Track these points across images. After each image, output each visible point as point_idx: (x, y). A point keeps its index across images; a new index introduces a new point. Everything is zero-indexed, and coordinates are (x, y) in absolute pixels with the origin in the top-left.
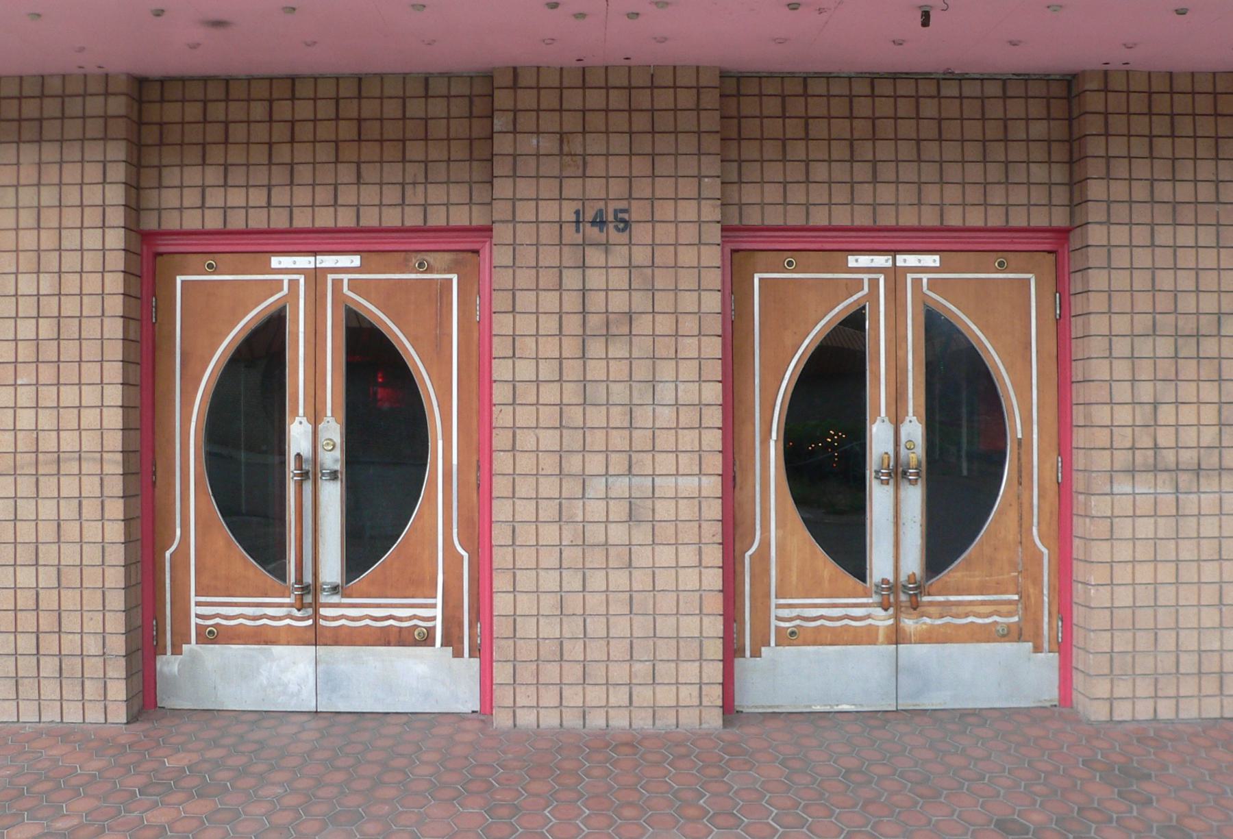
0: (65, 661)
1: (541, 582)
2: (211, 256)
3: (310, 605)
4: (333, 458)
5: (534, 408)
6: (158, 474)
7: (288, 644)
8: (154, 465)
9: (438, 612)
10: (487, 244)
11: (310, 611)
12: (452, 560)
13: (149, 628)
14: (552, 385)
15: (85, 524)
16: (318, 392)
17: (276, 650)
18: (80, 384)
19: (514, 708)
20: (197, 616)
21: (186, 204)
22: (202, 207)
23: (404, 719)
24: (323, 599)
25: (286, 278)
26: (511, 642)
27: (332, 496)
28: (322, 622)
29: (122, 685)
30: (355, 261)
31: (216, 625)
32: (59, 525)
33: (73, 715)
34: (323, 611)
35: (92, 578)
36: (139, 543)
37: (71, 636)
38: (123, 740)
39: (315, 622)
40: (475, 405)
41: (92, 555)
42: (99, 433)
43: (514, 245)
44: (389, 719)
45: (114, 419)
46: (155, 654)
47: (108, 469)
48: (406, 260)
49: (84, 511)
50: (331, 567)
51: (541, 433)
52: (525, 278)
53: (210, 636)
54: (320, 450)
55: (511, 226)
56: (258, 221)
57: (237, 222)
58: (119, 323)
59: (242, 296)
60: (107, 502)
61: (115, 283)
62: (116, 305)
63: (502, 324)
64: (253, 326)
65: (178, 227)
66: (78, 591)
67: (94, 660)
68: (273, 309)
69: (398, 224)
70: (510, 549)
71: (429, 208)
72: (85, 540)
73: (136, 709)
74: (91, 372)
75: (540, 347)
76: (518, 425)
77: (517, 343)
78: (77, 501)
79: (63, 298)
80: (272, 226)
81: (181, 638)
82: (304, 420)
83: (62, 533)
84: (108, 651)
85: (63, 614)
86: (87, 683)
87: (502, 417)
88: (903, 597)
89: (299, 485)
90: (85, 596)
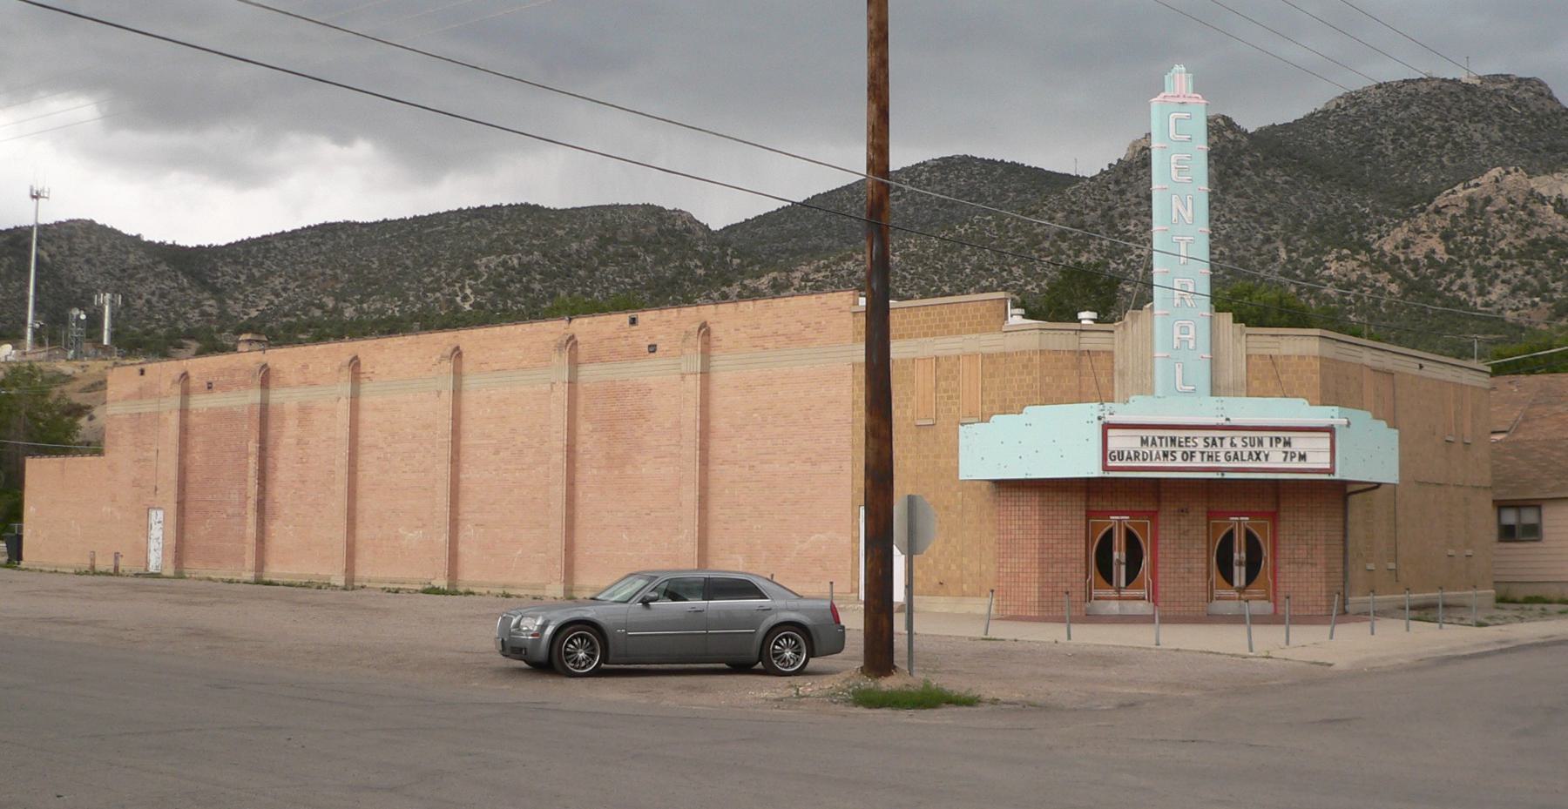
4: (1123, 560)
27: (1123, 568)
50: (1123, 584)
59: (1104, 525)
88: (1241, 590)
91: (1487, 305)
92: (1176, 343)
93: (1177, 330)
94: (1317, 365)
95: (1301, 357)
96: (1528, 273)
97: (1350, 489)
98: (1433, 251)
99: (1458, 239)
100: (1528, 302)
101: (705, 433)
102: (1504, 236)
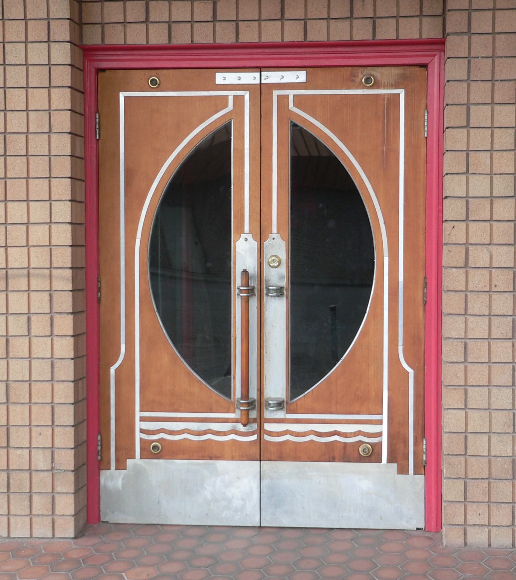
0: (13, 476)
1: (493, 399)
2: (154, 72)
3: (254, 421)
4: (278, 275)
5: (487, 224)
6: (103, 291)
7: (233, 459)
8: (99, 281)
9: (384, 428)
10: (436, 59)
11: (255, 426)
12: (398, 378)
13: (96, 442)
14: (506, 201)
15: (34, 340)
16: (264, 209)
17: (221, 465)
18: (27, 200)
19: (465, 526)
20: (142, 431)
21: (129, 19)
22: (147, 21)
23: (349, 535)
24: (267, 414)
25: (231, 94)
26: (462, 459)
27: (277, 313)
28: (267, 438)
29: (71, 499)
30: (301, 76)
31: (161, 440)
32: (7, 341)
33: (20, 530)
34: (268, 427)
35: (41, 393)
36: (85, 359)
37: (19, 452)
38: (75, 555)
39: (260, 438)
40: (422, 222)
41: (41, 370)
42: (48, 249)
43: (469, 58)
44: (335, 534)
45: (63, 235)
46: (100, 469)
47: (58, 285)
48: (354, 75)
49: (33, 326)
50: (277, 384)
51: (495, 250)
52: (480, 91)
53: (156, 451)
54: (265, 266)
55: (466, 38)
56: (204, 36)
57: (182, 37)
58: (68, 138)
60: (57, 318)
61: (62, 99)
62: (63, 121)
63: (455, 140)
64: (197, 143)
65: (122, 42)
66: (27, 407)
67: (42, 474)
68: (219, 126)
69: (346, 38)
70: (462, 366)
71: (378, 21)
72: (34, 356)
73: (82, 522)
74: (39, 189)
75: (495, 161)
76: (471, 241)
77: (470, 159)
78: (26, 317)
79: (8, 114)
80: (218, 41)
81: (125, 453)
82: (250, 237)
83: (10, 348)
84: (57, 466)
85: (12, 429)
86: (35, 498)
87: (453, 233)
89: (246, 302)
90: (33, 411)
101: (306, 143)
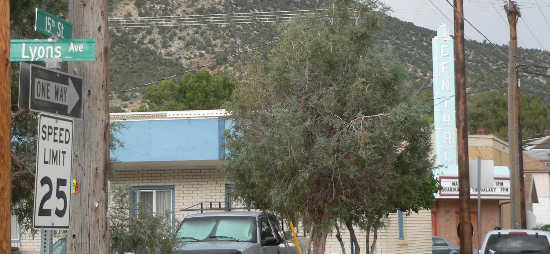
91: (168, 54)
92: (444, 141)
93: (444, 136)
94: (491, 150)
95: (486, 147)
96: (196, 33)
97: (500, 202)
98: (130, 15)
99: (148, 6)
100: (198, 53)
102: (180, 5)
